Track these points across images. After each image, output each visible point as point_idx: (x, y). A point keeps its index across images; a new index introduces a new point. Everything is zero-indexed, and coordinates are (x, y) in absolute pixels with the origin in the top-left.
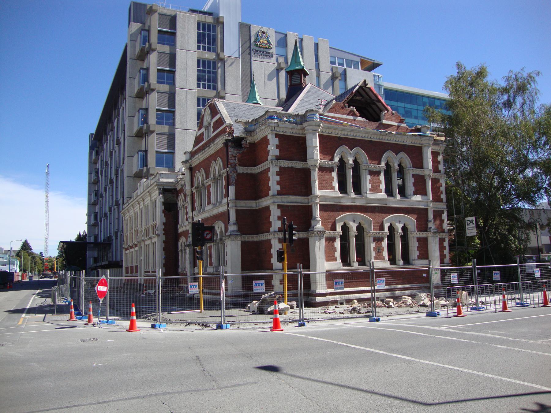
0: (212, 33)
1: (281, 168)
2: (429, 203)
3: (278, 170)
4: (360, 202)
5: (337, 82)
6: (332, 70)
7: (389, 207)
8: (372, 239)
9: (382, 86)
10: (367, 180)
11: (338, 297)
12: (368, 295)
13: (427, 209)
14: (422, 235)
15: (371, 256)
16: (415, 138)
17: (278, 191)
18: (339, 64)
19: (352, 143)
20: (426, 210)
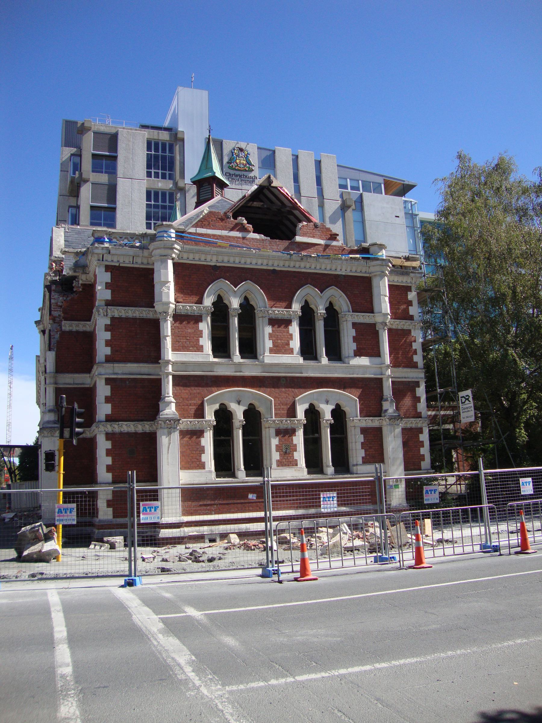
0: (167, 154)
1: (113, 319)
2: (384, 369)
3: (109, 322)
4: (250, 369)
5: (349, 214)
6: (342, 196)
7: (306, 378)
8: (273, 431)
9: (416, 215)
10: (265, 334)
11: (205, 530)
12: (260, 527)
13: (381, 380)
14: (372, 422)
15: (271, 459)
16: (356, 263)
17: (106, 356)
18: (353, 188)
19: (237, 275)
20: (378, 382)
